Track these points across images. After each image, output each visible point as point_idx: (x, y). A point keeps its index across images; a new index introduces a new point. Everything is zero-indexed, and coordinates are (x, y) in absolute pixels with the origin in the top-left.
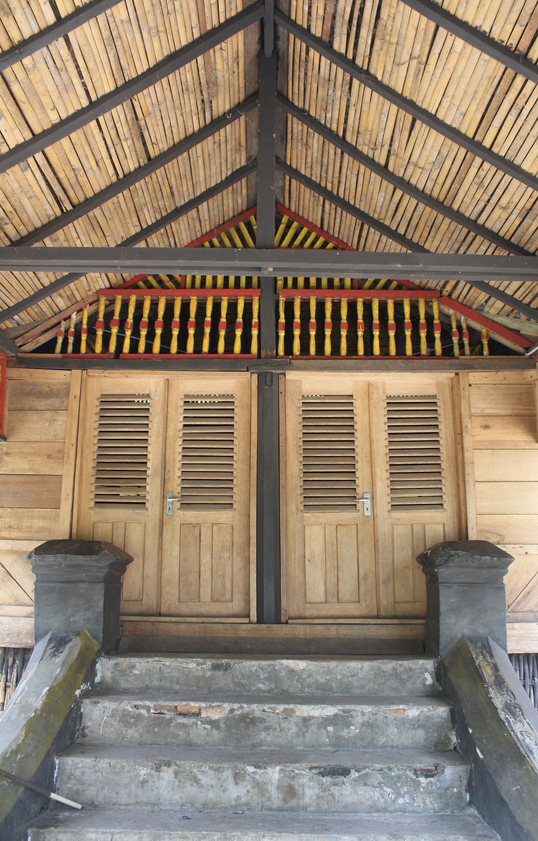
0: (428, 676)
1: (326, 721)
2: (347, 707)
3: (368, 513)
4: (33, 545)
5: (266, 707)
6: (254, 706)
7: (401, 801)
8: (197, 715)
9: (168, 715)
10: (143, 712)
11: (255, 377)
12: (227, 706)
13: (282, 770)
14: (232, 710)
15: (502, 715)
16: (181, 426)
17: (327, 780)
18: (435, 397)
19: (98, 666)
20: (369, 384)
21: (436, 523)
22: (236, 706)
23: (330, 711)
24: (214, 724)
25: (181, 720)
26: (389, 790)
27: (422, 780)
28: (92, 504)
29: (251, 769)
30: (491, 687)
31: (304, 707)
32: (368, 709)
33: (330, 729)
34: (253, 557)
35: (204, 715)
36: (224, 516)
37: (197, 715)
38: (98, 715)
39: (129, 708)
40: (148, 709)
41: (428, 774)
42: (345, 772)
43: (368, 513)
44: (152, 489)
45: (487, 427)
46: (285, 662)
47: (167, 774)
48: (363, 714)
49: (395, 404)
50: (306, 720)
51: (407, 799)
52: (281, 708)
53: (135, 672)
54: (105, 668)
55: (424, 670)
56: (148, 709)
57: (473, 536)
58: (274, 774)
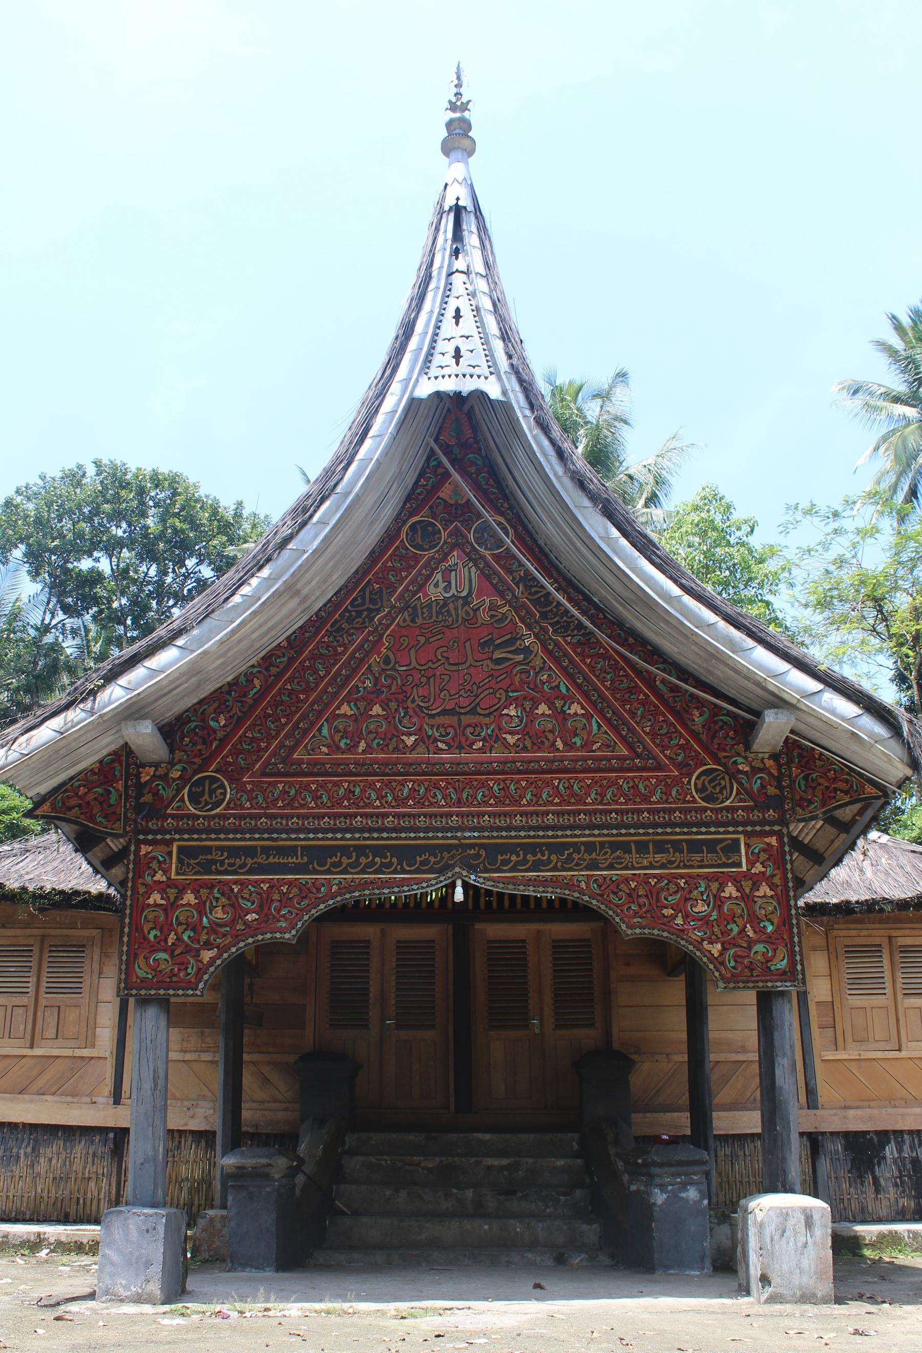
0: (574, 1144)
1: (502, 1168)
2: (517, 1159)
3: (537, 1031)
4: (292, 1058)
5: (463, 1159)
6: (456, 1158)
7: (548, 1210)
8: (418, 1164)
9: (399, 1164)
10: (383, 1163)
11: (451, 927)
12: (438, 1159)
13: (473, 1192)
14: (441, 1161)
15: (612, 1158)
16: (394, 965)
17: (502, 1198)
18: (589, 940)
19: (347, 1138)
20: (539, 931)
21: (588, 1037)
22: (443, 1159)
23: (505, 1162)
24: (430, 1170)
25: (407, 1168)
26: (540, 1204)
27: (562, 1198)
28: (328, 1026)
29: (455, 1191)
30: (67, 561)
31: (488, 1159)
32: (530, 1160)
33: (506, 1173)
34: (452, 1064)
35: (422, 1164)
36: (429, 1034)
37: (418, 1164)
38: (353, 1164)
39: (374, 1160)
40: (386, 1161)
41: (565, 1194)
42: (514, 1193)
43: (537, 1031)
44: (374, 1014)
45: (628, 964)
46: (475, 1135)
47: (403, 1194)
48: (527, 1163)
49: (558, 946)
50: (490, 1168)
51: (552, 1209)
52: (474, 1159)
53: (373, 1142)
54: (350, 1140)
55: (573, 1141)
56: (386, 1161)
57: (616, 1046)
58: (469, 1193)
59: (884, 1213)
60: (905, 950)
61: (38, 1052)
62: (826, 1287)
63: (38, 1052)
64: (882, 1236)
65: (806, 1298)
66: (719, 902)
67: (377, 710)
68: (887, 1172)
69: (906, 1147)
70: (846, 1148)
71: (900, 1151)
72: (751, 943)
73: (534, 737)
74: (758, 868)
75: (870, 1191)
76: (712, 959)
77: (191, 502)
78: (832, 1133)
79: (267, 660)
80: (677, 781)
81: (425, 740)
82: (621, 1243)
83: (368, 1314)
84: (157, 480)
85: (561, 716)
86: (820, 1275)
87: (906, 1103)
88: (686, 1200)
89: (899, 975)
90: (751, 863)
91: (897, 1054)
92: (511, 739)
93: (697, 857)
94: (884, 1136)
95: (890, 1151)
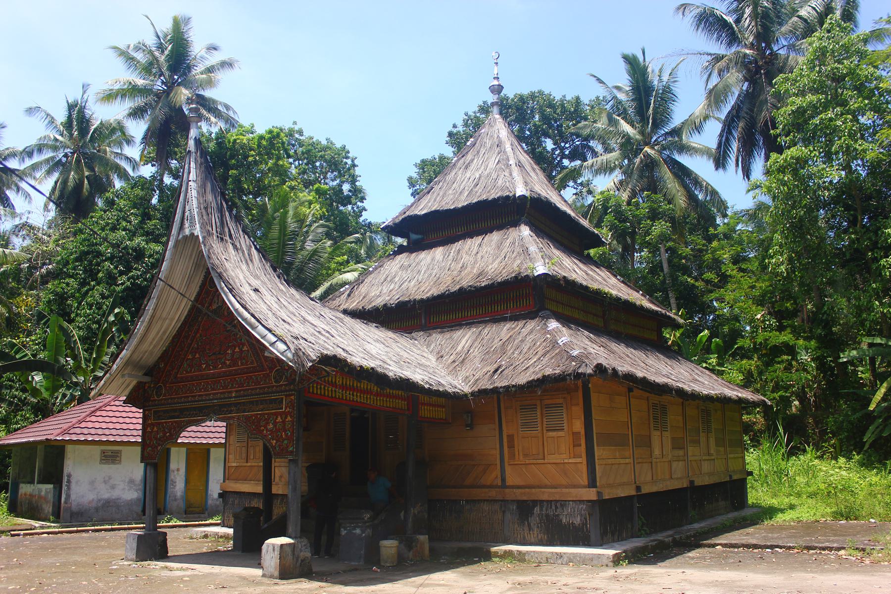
59: (533, 540)
60: (548, 406)
61: (249, 464)
62: (277, 574)
63: (249, 464)
64: (505, 552)
65: (272, 577)
66: (275, 423)
67: (197, 356)
68: (534, 520)
69: (544, 509)
70: (518, 508)
71: (541, 510)
72: (284, 440)
73: (234, 362)
74: (288, 409)
75: (526, 528)
76: (272, 446)
77: (551, 105)
78: (512, 501)
79: (173, 341)
80: (268, 374)
81: (208, 365)
82: (463, 547)
83: (177, 569)
84: (533, 96)
85: (241, 351)
86: (276, 568)
87: (546, 487)
88: (355, 534)
89: (545, 420)
90: (286, 408)
91: (542, 461)
92: (228, 362)
93: (271, 406)
94: (535, 502)
95: (537, 510)
